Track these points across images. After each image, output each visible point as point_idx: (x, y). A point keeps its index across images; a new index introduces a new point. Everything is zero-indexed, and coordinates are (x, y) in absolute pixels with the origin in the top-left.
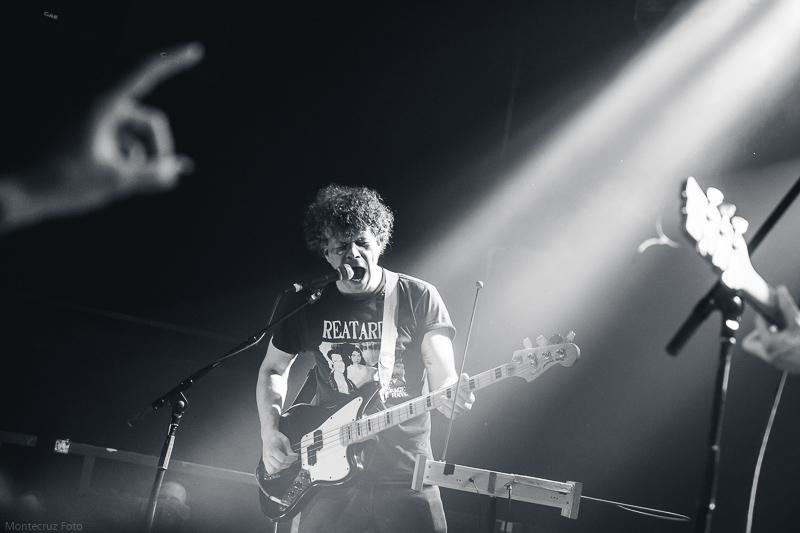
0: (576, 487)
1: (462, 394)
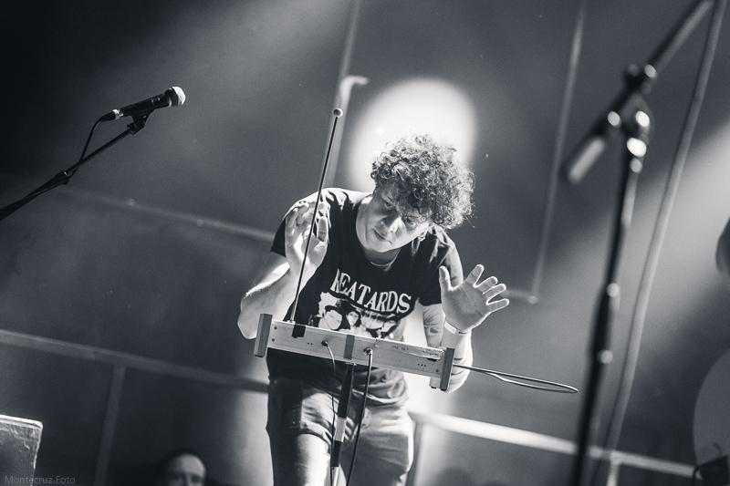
1: (278, 318)
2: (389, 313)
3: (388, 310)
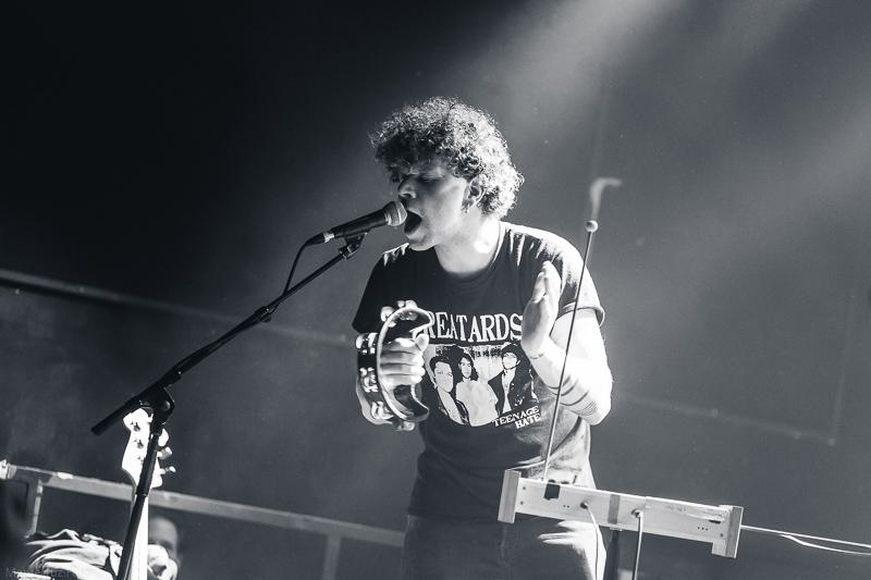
0: (732, 514)
2: (501, 342)
3: (499, 338)
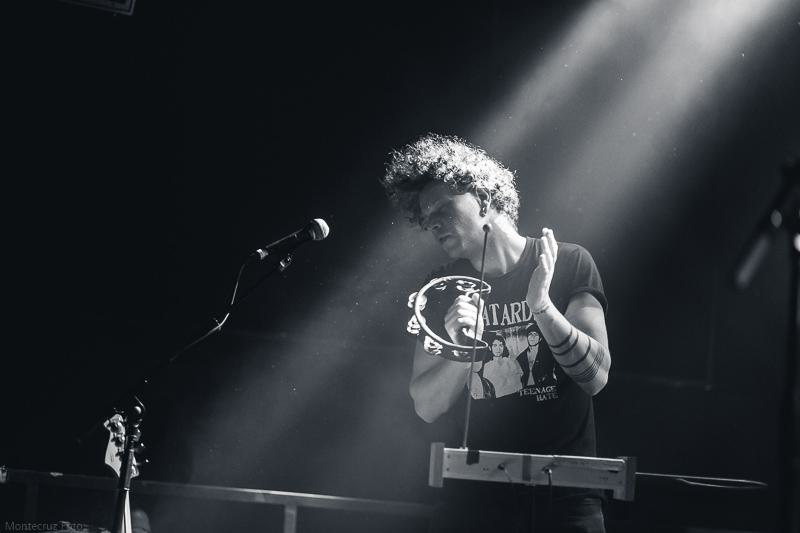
2: (527, 323)
3: (525, 320)
